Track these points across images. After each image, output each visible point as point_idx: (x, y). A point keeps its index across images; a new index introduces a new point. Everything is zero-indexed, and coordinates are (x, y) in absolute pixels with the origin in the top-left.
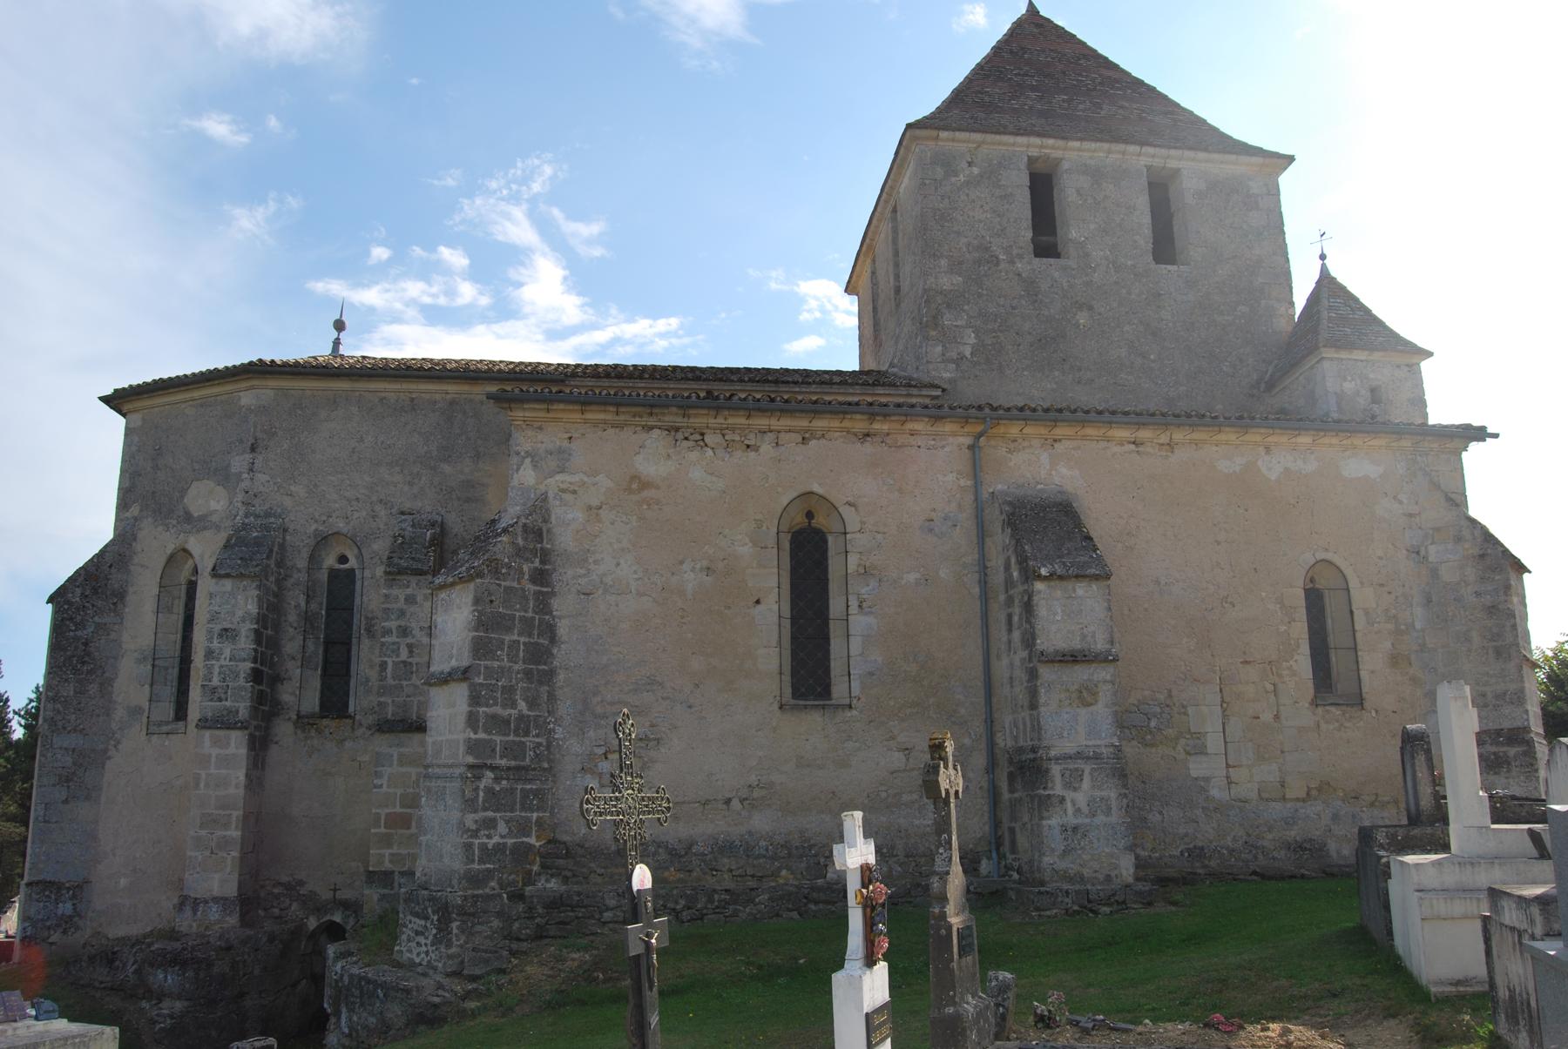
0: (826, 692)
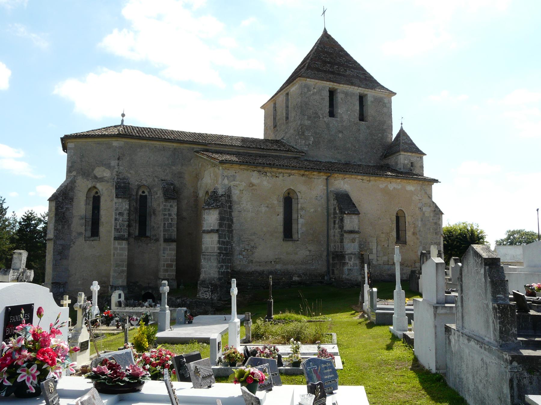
0: (291, 237)
